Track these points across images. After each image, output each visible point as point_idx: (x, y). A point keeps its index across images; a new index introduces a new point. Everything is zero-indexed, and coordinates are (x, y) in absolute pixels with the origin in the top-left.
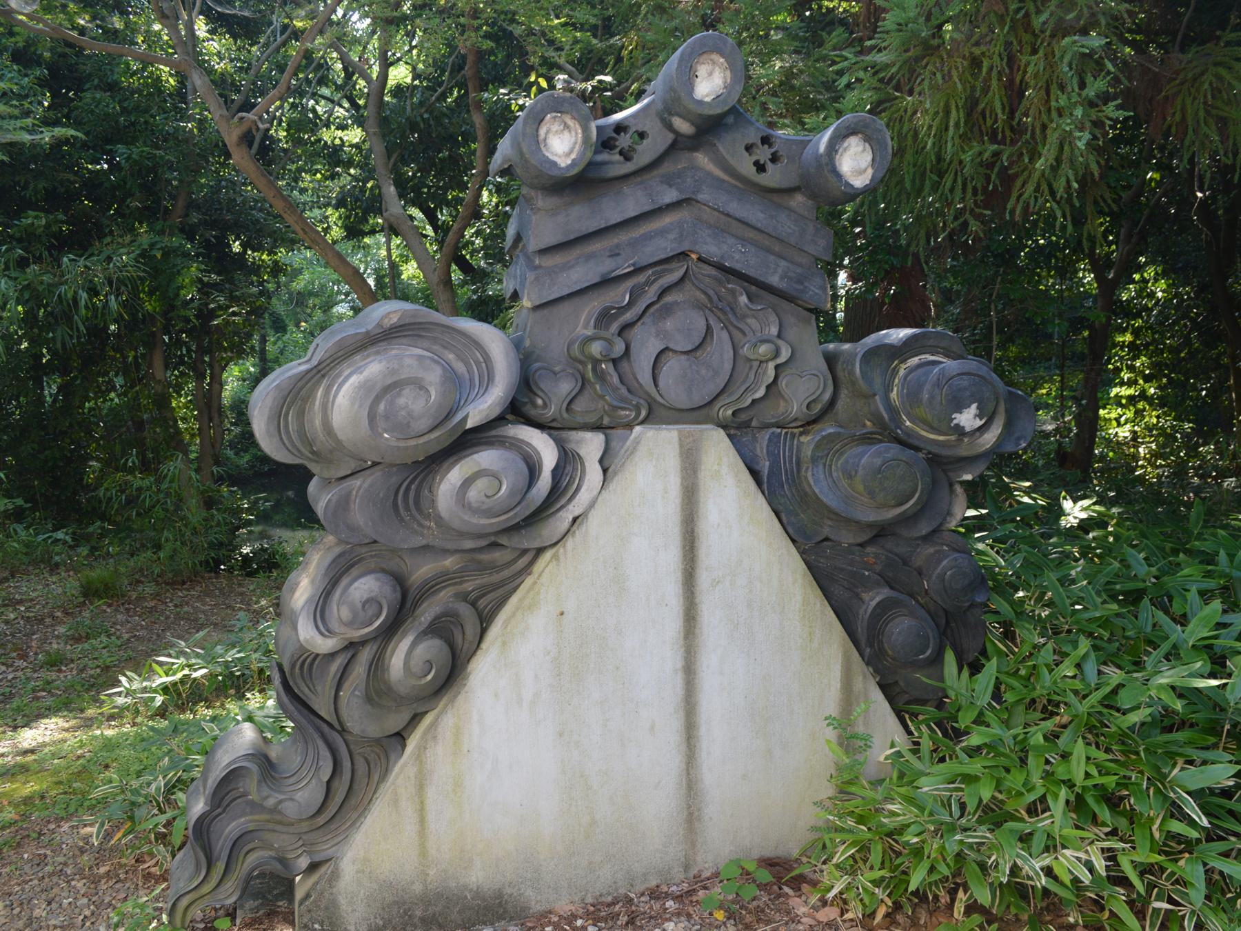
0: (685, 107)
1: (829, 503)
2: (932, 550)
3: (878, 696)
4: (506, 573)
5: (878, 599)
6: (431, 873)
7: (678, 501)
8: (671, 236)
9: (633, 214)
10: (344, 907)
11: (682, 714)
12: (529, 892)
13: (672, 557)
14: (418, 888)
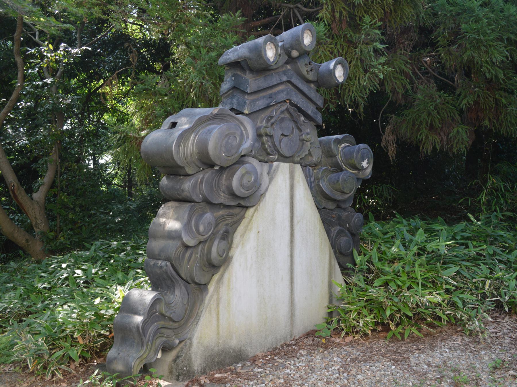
0: (301, 47)
1: (326, 192)
2: (347, 214)
3: (337, 266)
4: (238, 217)
5: (337, 230)
6: (220, 342)
7: (289, 190)
8: (285, 93)
9: (275, 83)
10: (193, 359)
11: (290, 273)
12: (249, 349)
13: (287, 211)
14: (216, 349)
